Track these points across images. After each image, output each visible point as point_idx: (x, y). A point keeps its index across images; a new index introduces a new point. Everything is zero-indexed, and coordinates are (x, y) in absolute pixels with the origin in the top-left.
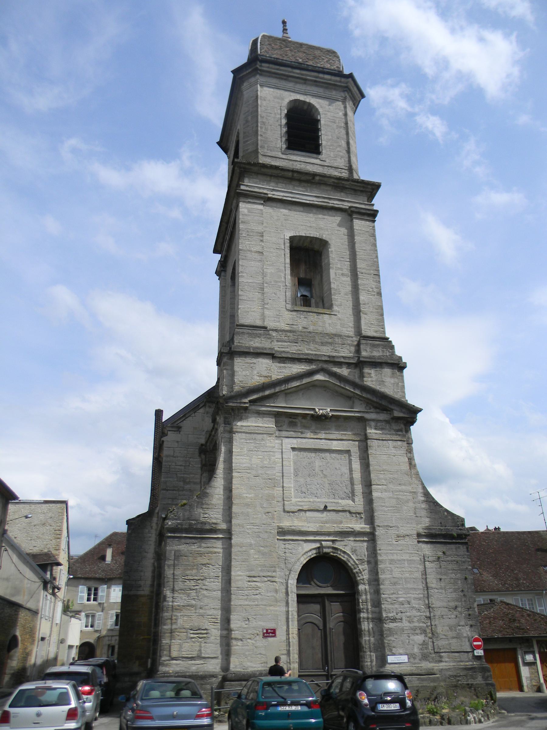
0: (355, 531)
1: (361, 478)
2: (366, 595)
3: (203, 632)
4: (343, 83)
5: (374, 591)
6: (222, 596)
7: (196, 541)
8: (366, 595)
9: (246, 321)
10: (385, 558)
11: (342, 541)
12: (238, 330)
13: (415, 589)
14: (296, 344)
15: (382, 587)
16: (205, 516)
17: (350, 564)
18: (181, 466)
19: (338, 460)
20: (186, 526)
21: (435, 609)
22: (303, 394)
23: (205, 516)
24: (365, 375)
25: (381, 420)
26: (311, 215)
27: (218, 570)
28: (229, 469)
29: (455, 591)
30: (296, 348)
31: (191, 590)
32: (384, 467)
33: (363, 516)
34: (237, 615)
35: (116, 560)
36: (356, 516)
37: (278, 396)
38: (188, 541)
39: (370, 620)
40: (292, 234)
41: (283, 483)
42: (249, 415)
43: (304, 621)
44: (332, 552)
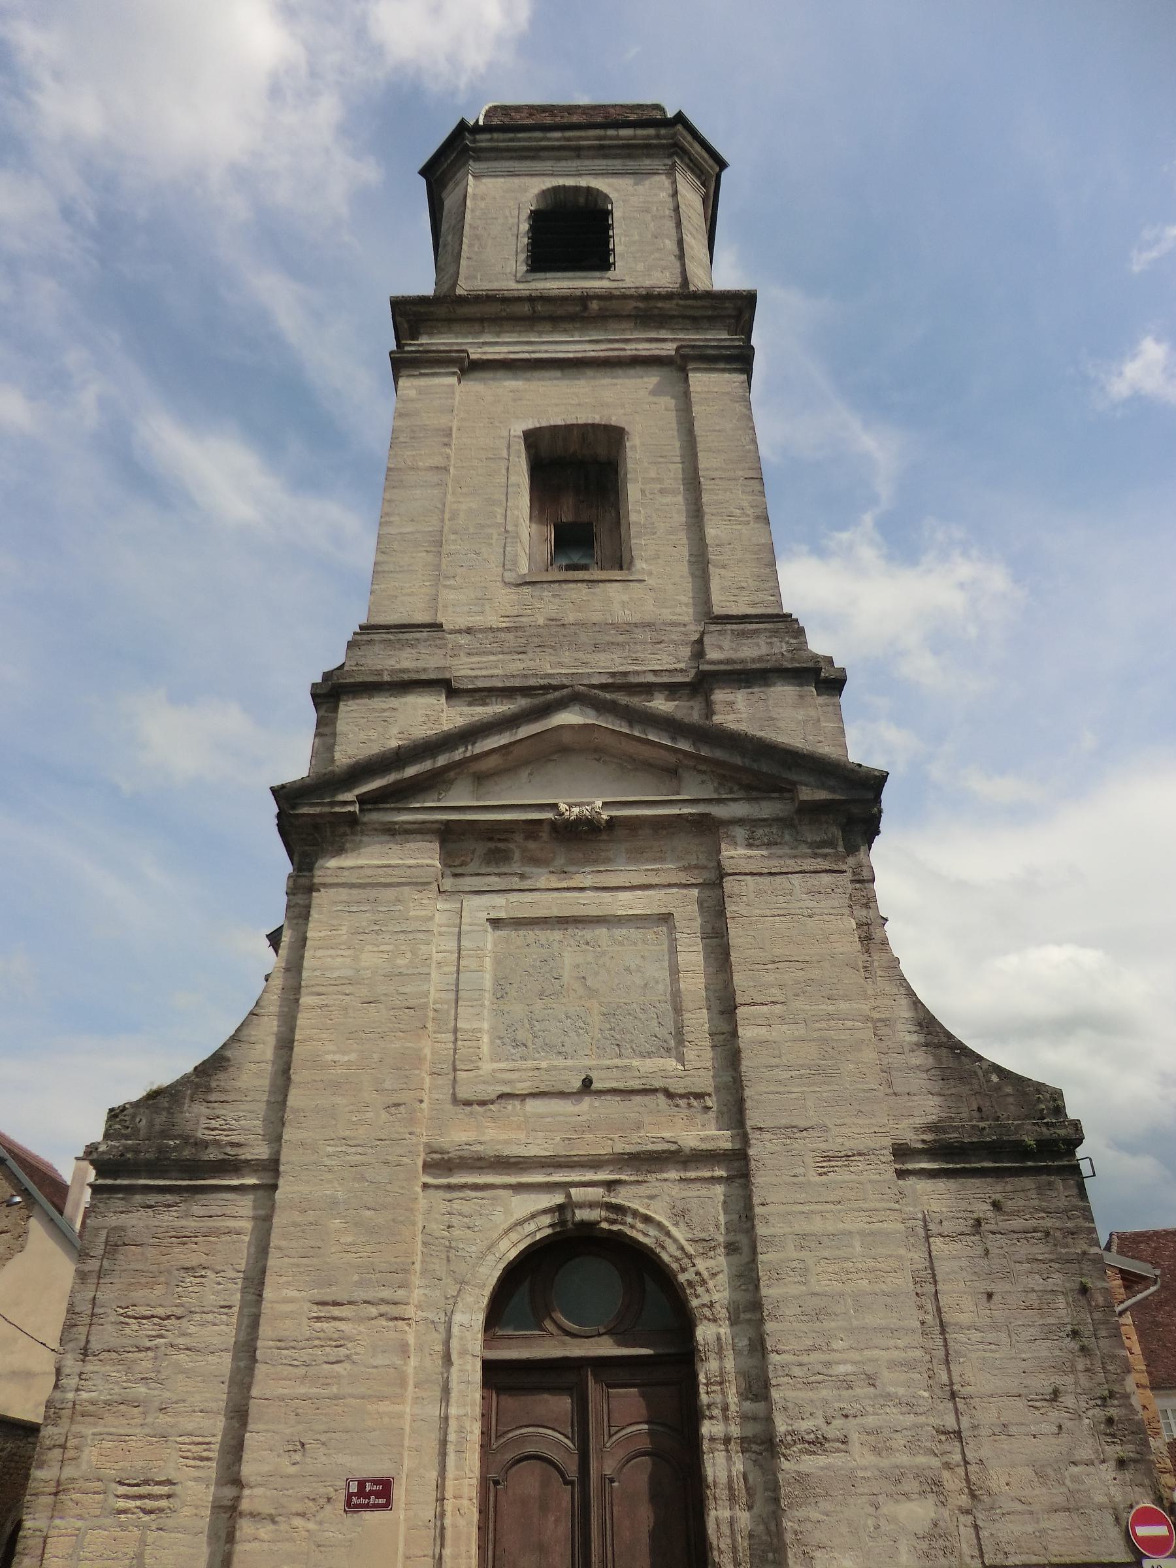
1: (707, 990)
2: (720, 1355)
7: (177, 1198)
8: (720, 1355)
9: (388, 618)
10: (782, 1231)
11: (638, 1182)
14: (521, 656)
15: (769, 1326)
16: (214, 1123)
17: (665, 1257)
19: (635, 944)
21: (975, 1402)
23: (214, 1123)
24: (718, 707)
26: (582, 382)
29: (1048, 1333)
30: (521, 666)
31: (140, 1351)
32: (777, 951)
33: (710, 1104)
34: (267, 1431)
36: (690, 1105)
37: (451, 782)
38: (153, 1199)
39: (734, 1447)
40: (530, 424)
41: (456, 1019)
42: (365, 839)
43: (509, 1456)
44: (607, 1220)
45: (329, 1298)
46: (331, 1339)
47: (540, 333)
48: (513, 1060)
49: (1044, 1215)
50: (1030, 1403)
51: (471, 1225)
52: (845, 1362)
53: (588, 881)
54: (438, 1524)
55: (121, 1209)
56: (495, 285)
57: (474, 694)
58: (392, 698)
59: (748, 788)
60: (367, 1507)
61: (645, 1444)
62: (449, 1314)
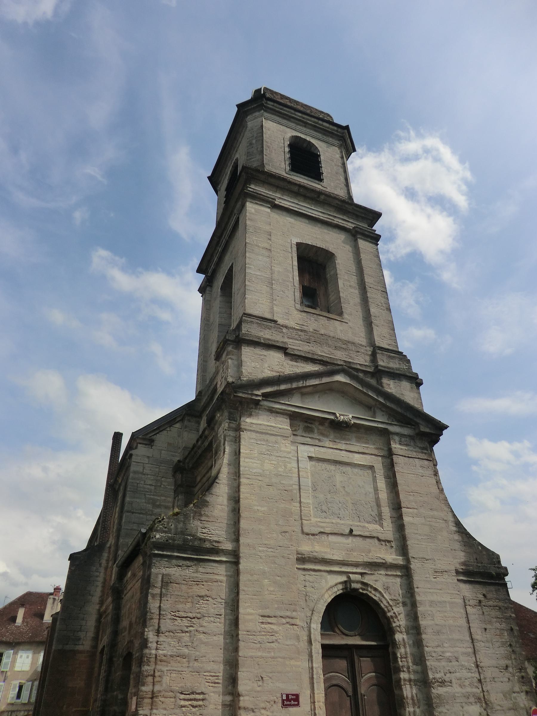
0: (386, 563)
2: (405, 647)
3: (198, 697)
4: (340, 132)
5: (413, 643)
6: (225, 644)
8: (405, 647)
12: (246, 319)
13: (461, 641)
14: (308, 344)
15: (424, 636)
16: (204, 531)
17: (382, 605)
18: (150, 485)
19: (361, 476)
20: (178, 542)
21: (484, 669)
22: (319, 397)
23: (204, 531)
25: (405, 435)
26: (317, 228)
27: (220, 605)
28: (236, 474)
30: (309, 349)
31: (183, 632)
33: (393, 545)
35: (27, 623)
37: (293, 394)
38: (181, 562)
39: (412, 683)
41: (300, 497)
42: (260, 412)
44: (362, 589)
45: (266, 614)
46: (269, 632)
47: (299, 201)
48: (322, 518)
49: (498, 601)
50: (500, 670)
51: (313, 586)
52: (448, 652)
53: (343, 447)
54: (313, 713)
55: (167, 566)
56: (277, 172)
57: (293, 356)
58: (264, 351)
59: (398, 421)
60: (290, 705)
61: (375, 681)
62: (308, 624)
